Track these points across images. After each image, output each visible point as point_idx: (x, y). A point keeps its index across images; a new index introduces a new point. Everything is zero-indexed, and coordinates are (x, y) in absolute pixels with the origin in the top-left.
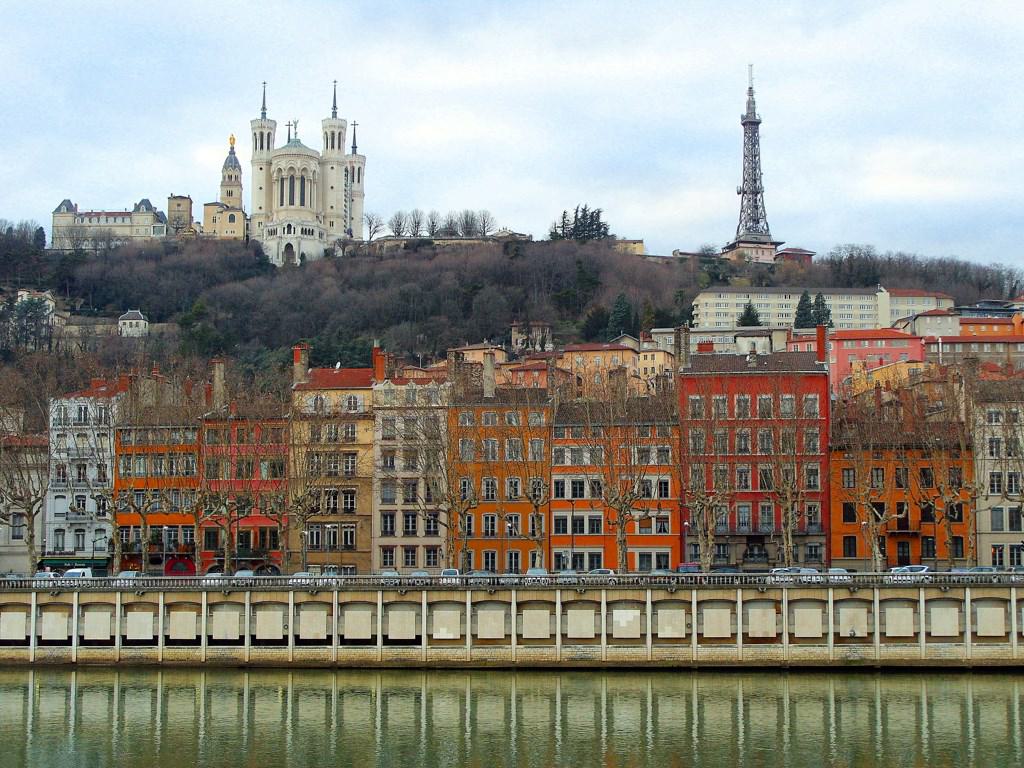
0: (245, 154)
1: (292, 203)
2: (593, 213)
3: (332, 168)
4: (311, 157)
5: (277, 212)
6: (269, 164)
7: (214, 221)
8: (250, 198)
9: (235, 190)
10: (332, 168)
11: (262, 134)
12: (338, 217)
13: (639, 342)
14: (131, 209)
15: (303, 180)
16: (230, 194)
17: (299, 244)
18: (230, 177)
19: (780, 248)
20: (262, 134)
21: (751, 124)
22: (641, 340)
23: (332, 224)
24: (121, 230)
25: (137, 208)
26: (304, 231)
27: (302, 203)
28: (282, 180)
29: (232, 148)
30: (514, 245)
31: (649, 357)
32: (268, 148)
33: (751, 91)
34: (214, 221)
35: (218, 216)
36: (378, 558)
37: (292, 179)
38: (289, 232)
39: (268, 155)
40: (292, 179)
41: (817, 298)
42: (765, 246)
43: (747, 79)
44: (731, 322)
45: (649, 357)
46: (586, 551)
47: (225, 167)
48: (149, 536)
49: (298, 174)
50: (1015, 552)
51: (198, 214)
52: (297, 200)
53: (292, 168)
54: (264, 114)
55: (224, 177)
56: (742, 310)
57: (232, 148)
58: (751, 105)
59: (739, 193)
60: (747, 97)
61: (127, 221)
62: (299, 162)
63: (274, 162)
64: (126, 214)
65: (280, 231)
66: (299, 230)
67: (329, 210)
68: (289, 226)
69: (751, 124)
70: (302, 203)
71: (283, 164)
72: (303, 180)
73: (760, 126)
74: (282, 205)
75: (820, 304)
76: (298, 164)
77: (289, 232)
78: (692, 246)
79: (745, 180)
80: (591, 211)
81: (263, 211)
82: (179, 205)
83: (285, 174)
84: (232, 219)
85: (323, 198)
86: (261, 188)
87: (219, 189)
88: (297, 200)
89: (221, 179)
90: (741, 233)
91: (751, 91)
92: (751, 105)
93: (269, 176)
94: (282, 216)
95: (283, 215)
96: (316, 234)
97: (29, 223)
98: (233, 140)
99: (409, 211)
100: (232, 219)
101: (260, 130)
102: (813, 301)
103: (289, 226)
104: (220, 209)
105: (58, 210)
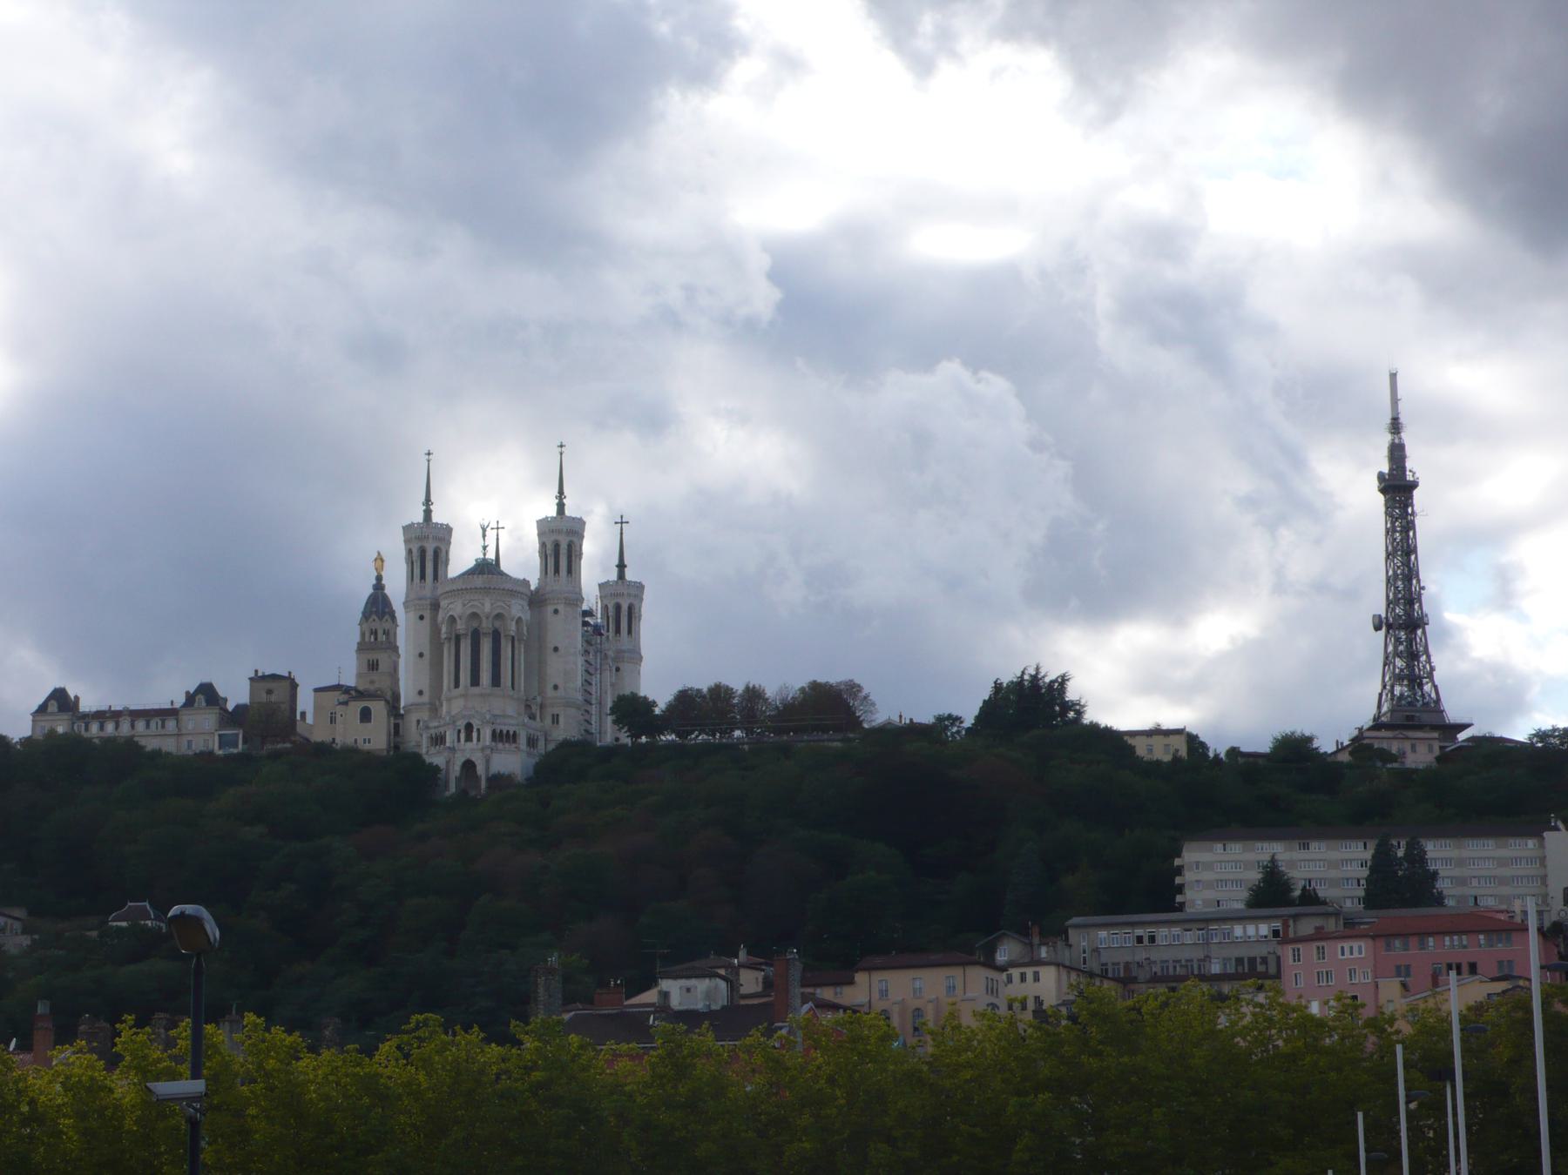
0: (397, 585)
1: (475, 681)
2: (1052, 682)
3: (556, 612)
4: (513, 593)
5: (449, 700)
6: (435, 606)
7: (333, 720)
8: (410, 682)
9: (383, 659)
10: (556, 612)
11: (423, 552)
12: (568, 704)
13: (1031, 945)
14: (180, 700)
15: (496, 636)
16: (373, 666)
17: (488, 762)
18: (374, 632)
19: (1462, 736)
20: (423, 552)
22: (1036, 940)
23: (555, 719)
24: (152, 739)
25: (190, 699)
26: (498, 736)
27: (496, 681)
28: (458, 638)
29: (379, 578)
31: (1030, 977)
32: (436, 577)
34: (333, 720)
35: (340, 709)
37: (476, 637)
38: (469, 738)
39: (435, 588)
40: (476, 637)
41: (1409, 846)
42: (1419, 734)
44: (1236, 900)
45: (1030, 977)
47: (366, 615)
49: (486, 625)
51: (305, 701)
53: (474, 615)
55: (363, 635)
56: (1255, 876)
57: (379, 578)
59: (1377, 628)
61: (171, 724)
63: (443, 603)
64: (171, 713)
65: (450, 739)
66: (487, 734)
67: (550, 692)
68: (469, 727)
70: (496, 681)
71: (456, 608)
72: (496, 636)
73: (1416, 493)
74: (457, 685)
75: (1417, 857)
76: (487, 606)
77: (469, 738)
79: (1389, 603)
80: (1047, 680)
81: (425, 698)
82: (269, 692)
83: (461, 626)
84: (366, 715)
85: (537, 669)
86: (421, 655)
87: (354, 655)
89: (357, 638)
90: (1385, 709)
93: (435, 630)
94: (457, 706)
95: (455, 706)
96: (522, 741)
97: (757, 686)
98: (380, 559)
100: (366, 715)
102: (1400, 853)
103: (469, 727)
104: (344, 698)
105: (42, 709)
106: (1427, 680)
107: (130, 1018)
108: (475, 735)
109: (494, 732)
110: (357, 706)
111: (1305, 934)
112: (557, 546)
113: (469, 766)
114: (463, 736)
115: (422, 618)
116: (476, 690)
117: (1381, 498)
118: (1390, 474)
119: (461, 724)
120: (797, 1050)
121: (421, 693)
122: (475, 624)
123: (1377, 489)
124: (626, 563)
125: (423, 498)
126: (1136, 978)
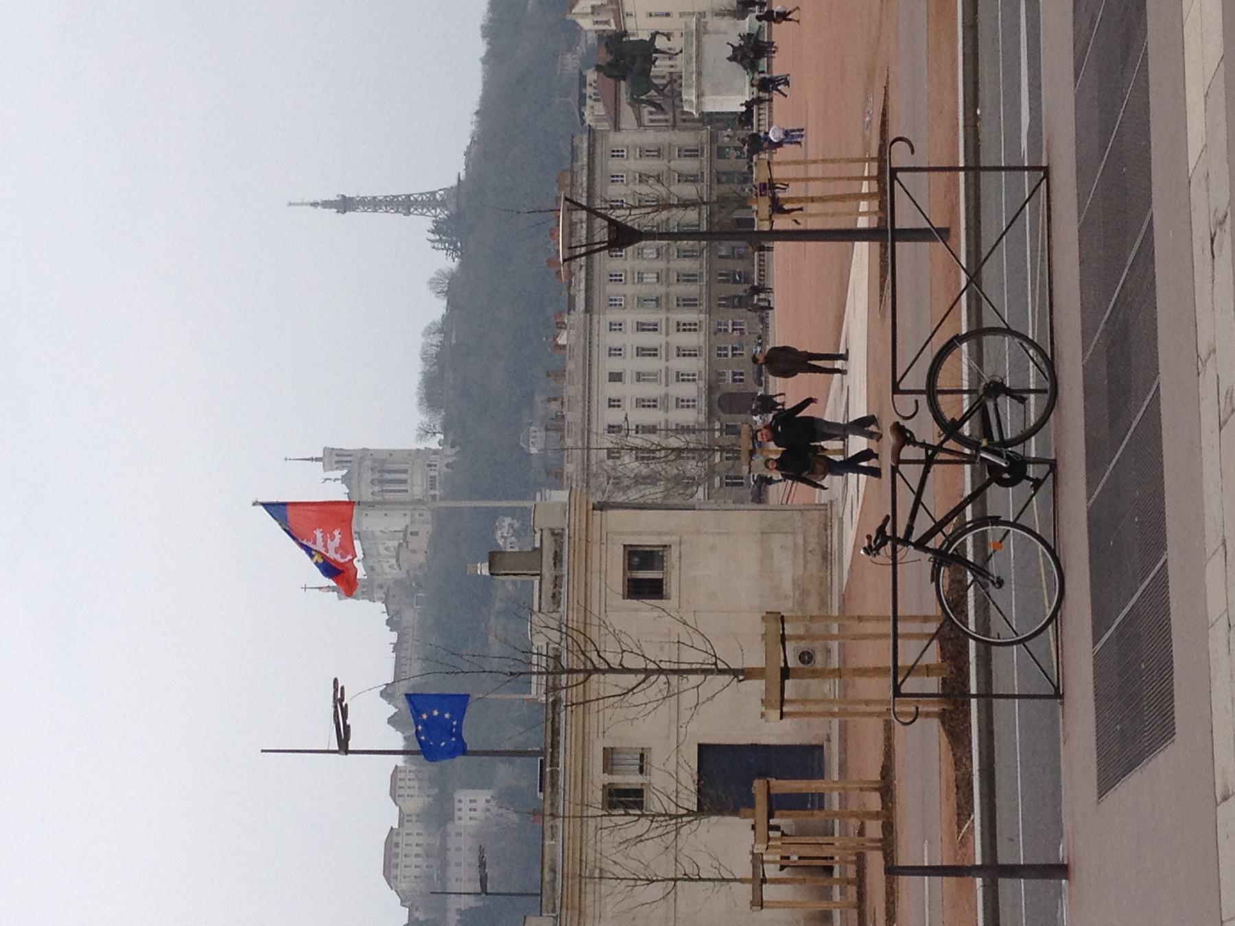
1: (405, 482)
15: (382, 471)
18: (363, 593)
21: (345, 205)
28: (382, 491)
30: (487, 53)
33: (315, 204)
36: (673, 589)
37: (381, 482)
43: (305, 208)
46: (625, 179)
48: (643, 221)
49: (377, 476)
50: (614, 455)
52: (404, 476)
54: (317, 459)
58: (326, 204)
60: (319, 208)
62: (365, 463)
65: (432, 473)
68: (429, 466)
69: (345, 205)
74: (407, 491)
78: (480, 47)
84: (415, 534)
86: (386, 515)
88: (404, 476)
91: (315, 204)
92: (326, 204)
99: (423, 340)
100: (415, 534)
101: (334, 464)
103: (429, 466)
106: (656, 81)
107: (517, 525)
108: (433, 463)
109: (431, 489)
110: (410, 538)
111: (877, 679)
112: (337, 462)
113: (448, 466)
114: (433, 468)
115: (367, 515)
116: (409, 481)
117: (348, 213)
118: (336, 208)
119: (427, 468)
120: (676, 471)
121: (405, 515)
122: (376, 482)
123: (345, 756)
124: (349, 755)
125: (310, 462)
126: (769, 180)
